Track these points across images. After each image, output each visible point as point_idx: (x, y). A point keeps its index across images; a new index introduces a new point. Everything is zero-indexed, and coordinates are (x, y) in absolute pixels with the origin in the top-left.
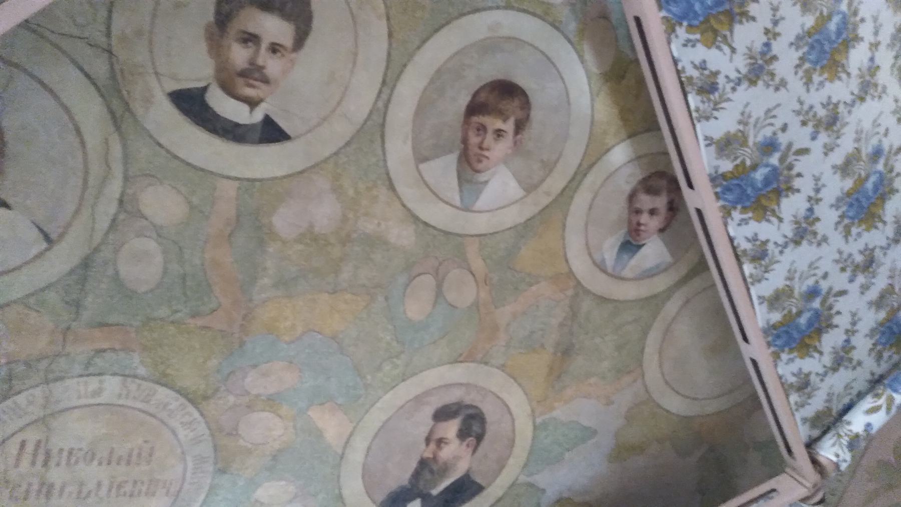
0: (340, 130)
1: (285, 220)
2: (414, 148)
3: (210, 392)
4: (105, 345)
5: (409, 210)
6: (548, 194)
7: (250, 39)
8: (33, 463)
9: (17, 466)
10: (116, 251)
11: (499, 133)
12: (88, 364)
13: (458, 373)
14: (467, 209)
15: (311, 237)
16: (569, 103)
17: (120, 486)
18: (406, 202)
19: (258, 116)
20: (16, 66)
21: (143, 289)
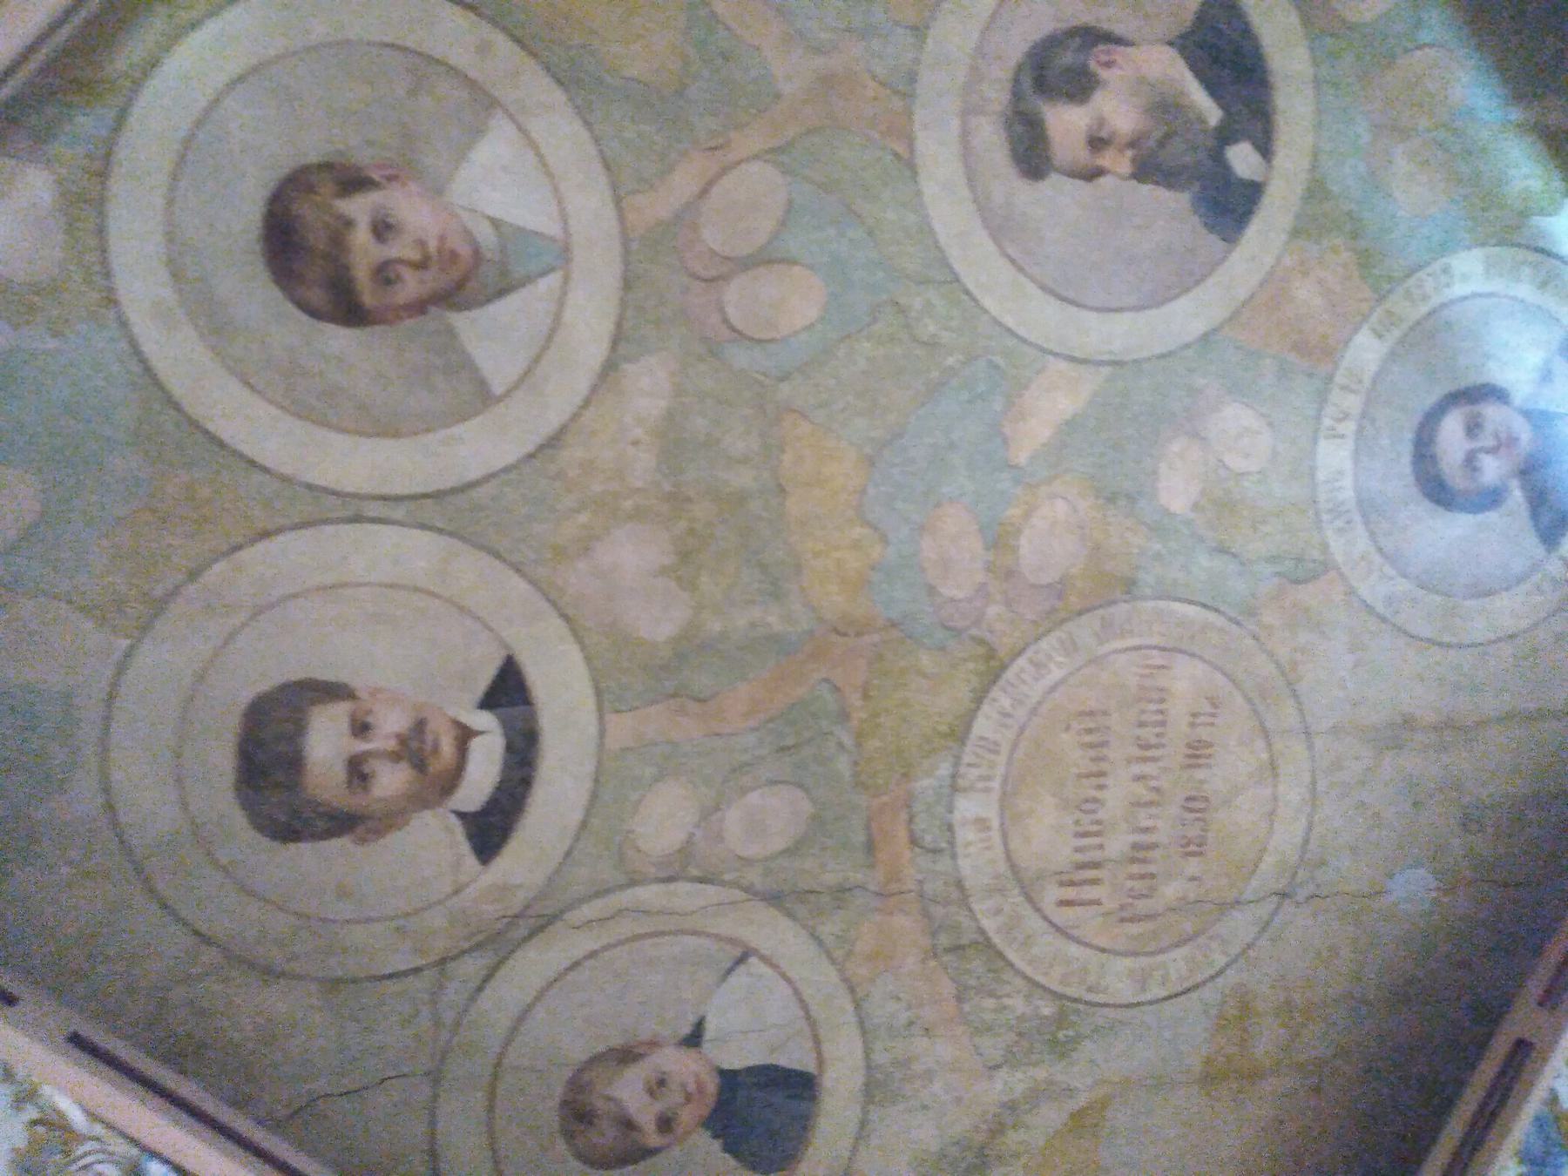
0: (471, 572)
1: (658, 622)
2: (464, 418)
3: (981, 650)
4: (902, 834)
5: (594, 389)
6: (484, 49)
7: (358, 772)
8: (1095, 882)
9: (1098, 903)
10: (748, 862)
11: (383, 229)
12: (936, 851)
13: (937, 151)
14: (565, 252)
15: (685, 563)
16: (255, 70)
17: (1148, 747)
18: (578, 401)
19: (485, 721)
20: (498, 1065)
21: (807, 807)
